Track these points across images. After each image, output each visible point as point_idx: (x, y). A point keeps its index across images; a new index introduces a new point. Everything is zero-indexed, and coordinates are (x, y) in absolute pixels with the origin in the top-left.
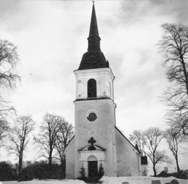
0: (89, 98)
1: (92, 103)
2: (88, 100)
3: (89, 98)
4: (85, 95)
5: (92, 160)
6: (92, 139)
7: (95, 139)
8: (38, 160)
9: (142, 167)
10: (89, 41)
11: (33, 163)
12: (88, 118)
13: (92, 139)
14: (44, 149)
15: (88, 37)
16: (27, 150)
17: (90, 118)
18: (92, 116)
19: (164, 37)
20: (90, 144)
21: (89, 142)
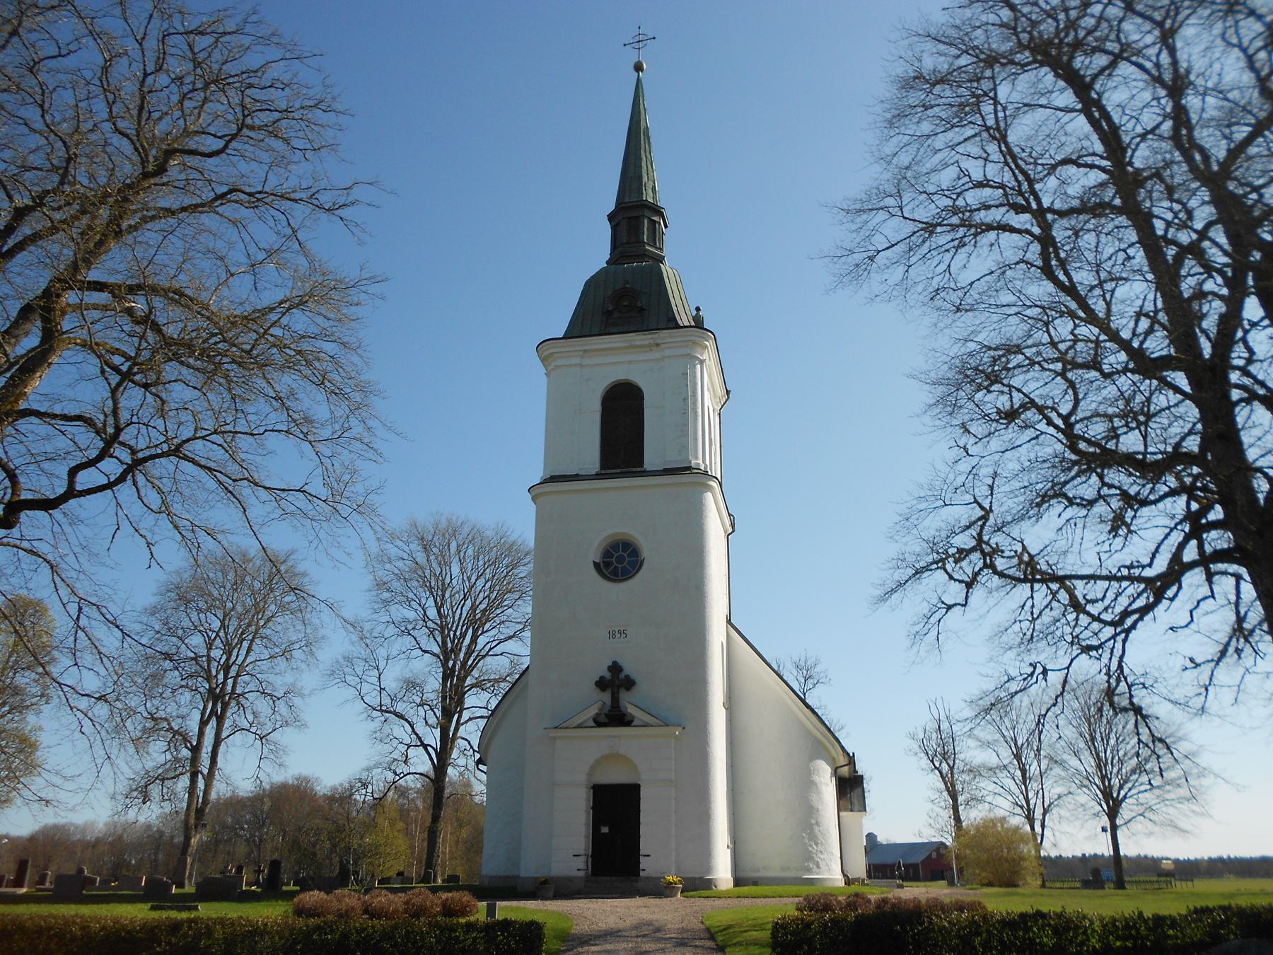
0: (603, 472)
1: (507, 566)
2: (598, 476)
3: (603, 472)
4: (591, 458)
5: (615, 776)
6: (615, 668)
7: (629, 669)
8: (934, 840)
9: (963, 864)
10: (615, 229)
11: (924, 901)
12: (596, 565)
13: (615, 668)
14: (1238, 613)
15: (611, 207)
16: (803, 659)
17: (607, 565)
18: (621, 559)
19: (887, 160)
20: (606, 697)
21: (601, 684)
